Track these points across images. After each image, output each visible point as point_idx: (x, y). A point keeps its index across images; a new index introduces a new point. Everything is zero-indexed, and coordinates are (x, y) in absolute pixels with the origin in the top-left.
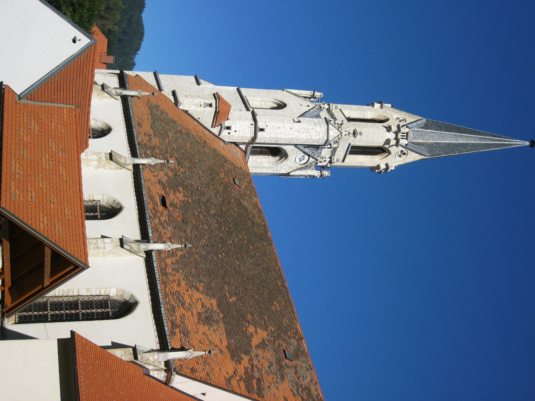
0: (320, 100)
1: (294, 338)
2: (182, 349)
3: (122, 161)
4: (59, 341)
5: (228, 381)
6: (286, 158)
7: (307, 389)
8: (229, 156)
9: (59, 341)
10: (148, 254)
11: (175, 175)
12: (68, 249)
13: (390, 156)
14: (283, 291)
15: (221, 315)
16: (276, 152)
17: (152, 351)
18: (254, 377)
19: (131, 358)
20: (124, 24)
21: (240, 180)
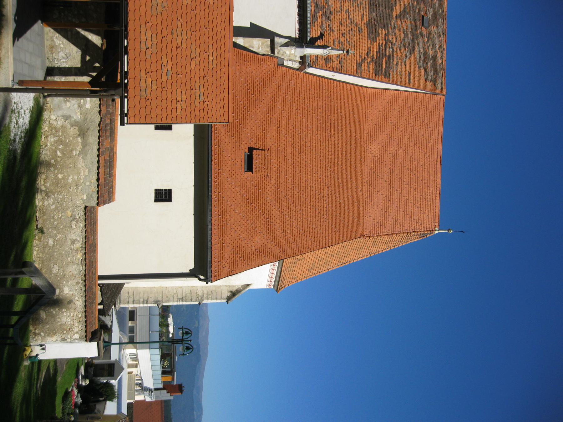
18: (385, 55)
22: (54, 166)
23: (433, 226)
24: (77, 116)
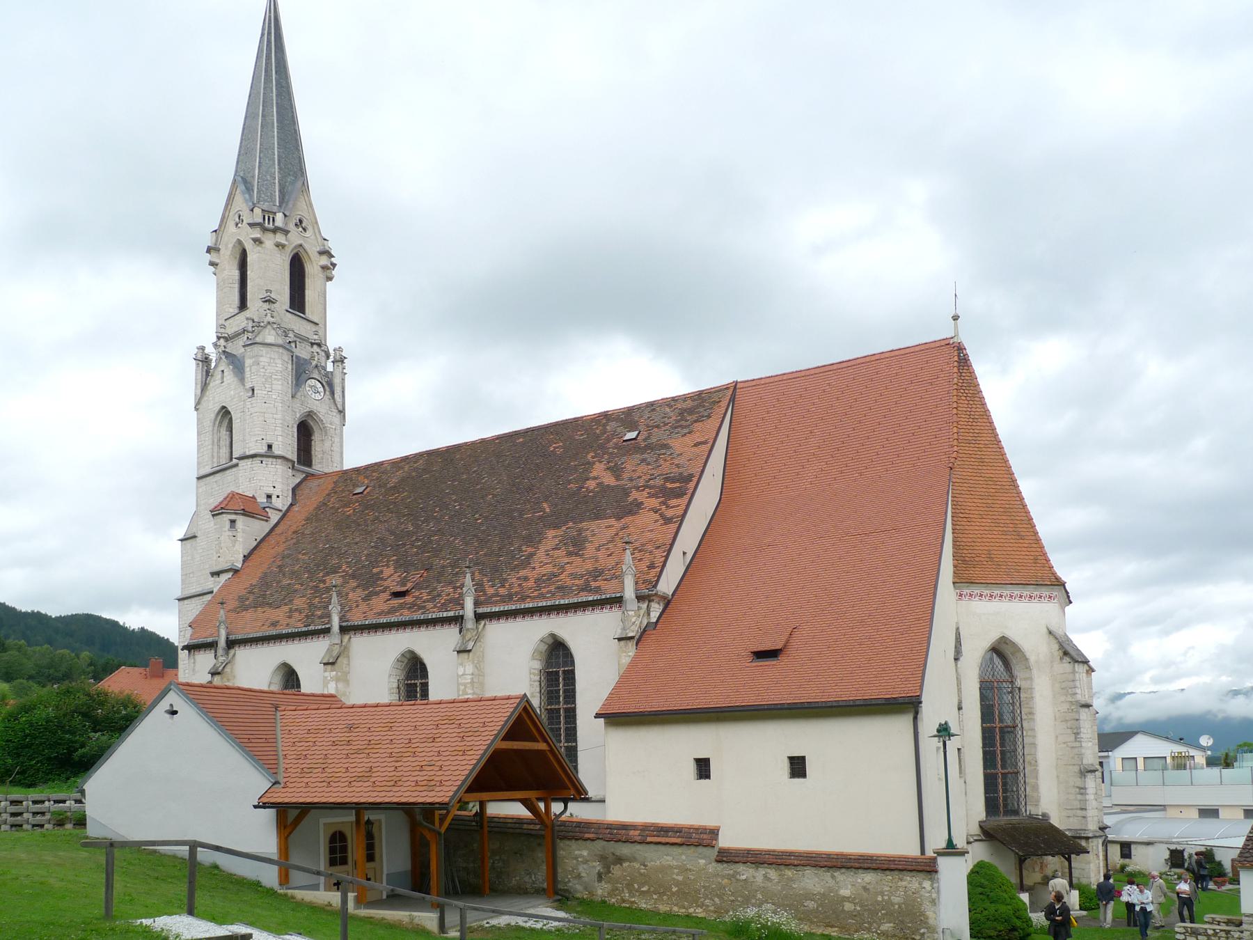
1: (604, 425)
3: (336, 650)
6: (1017, 649)
11: (353, 576)
12: (500, 719)
15: (571, 524)
21: (355, 486)
24: (598, 866)
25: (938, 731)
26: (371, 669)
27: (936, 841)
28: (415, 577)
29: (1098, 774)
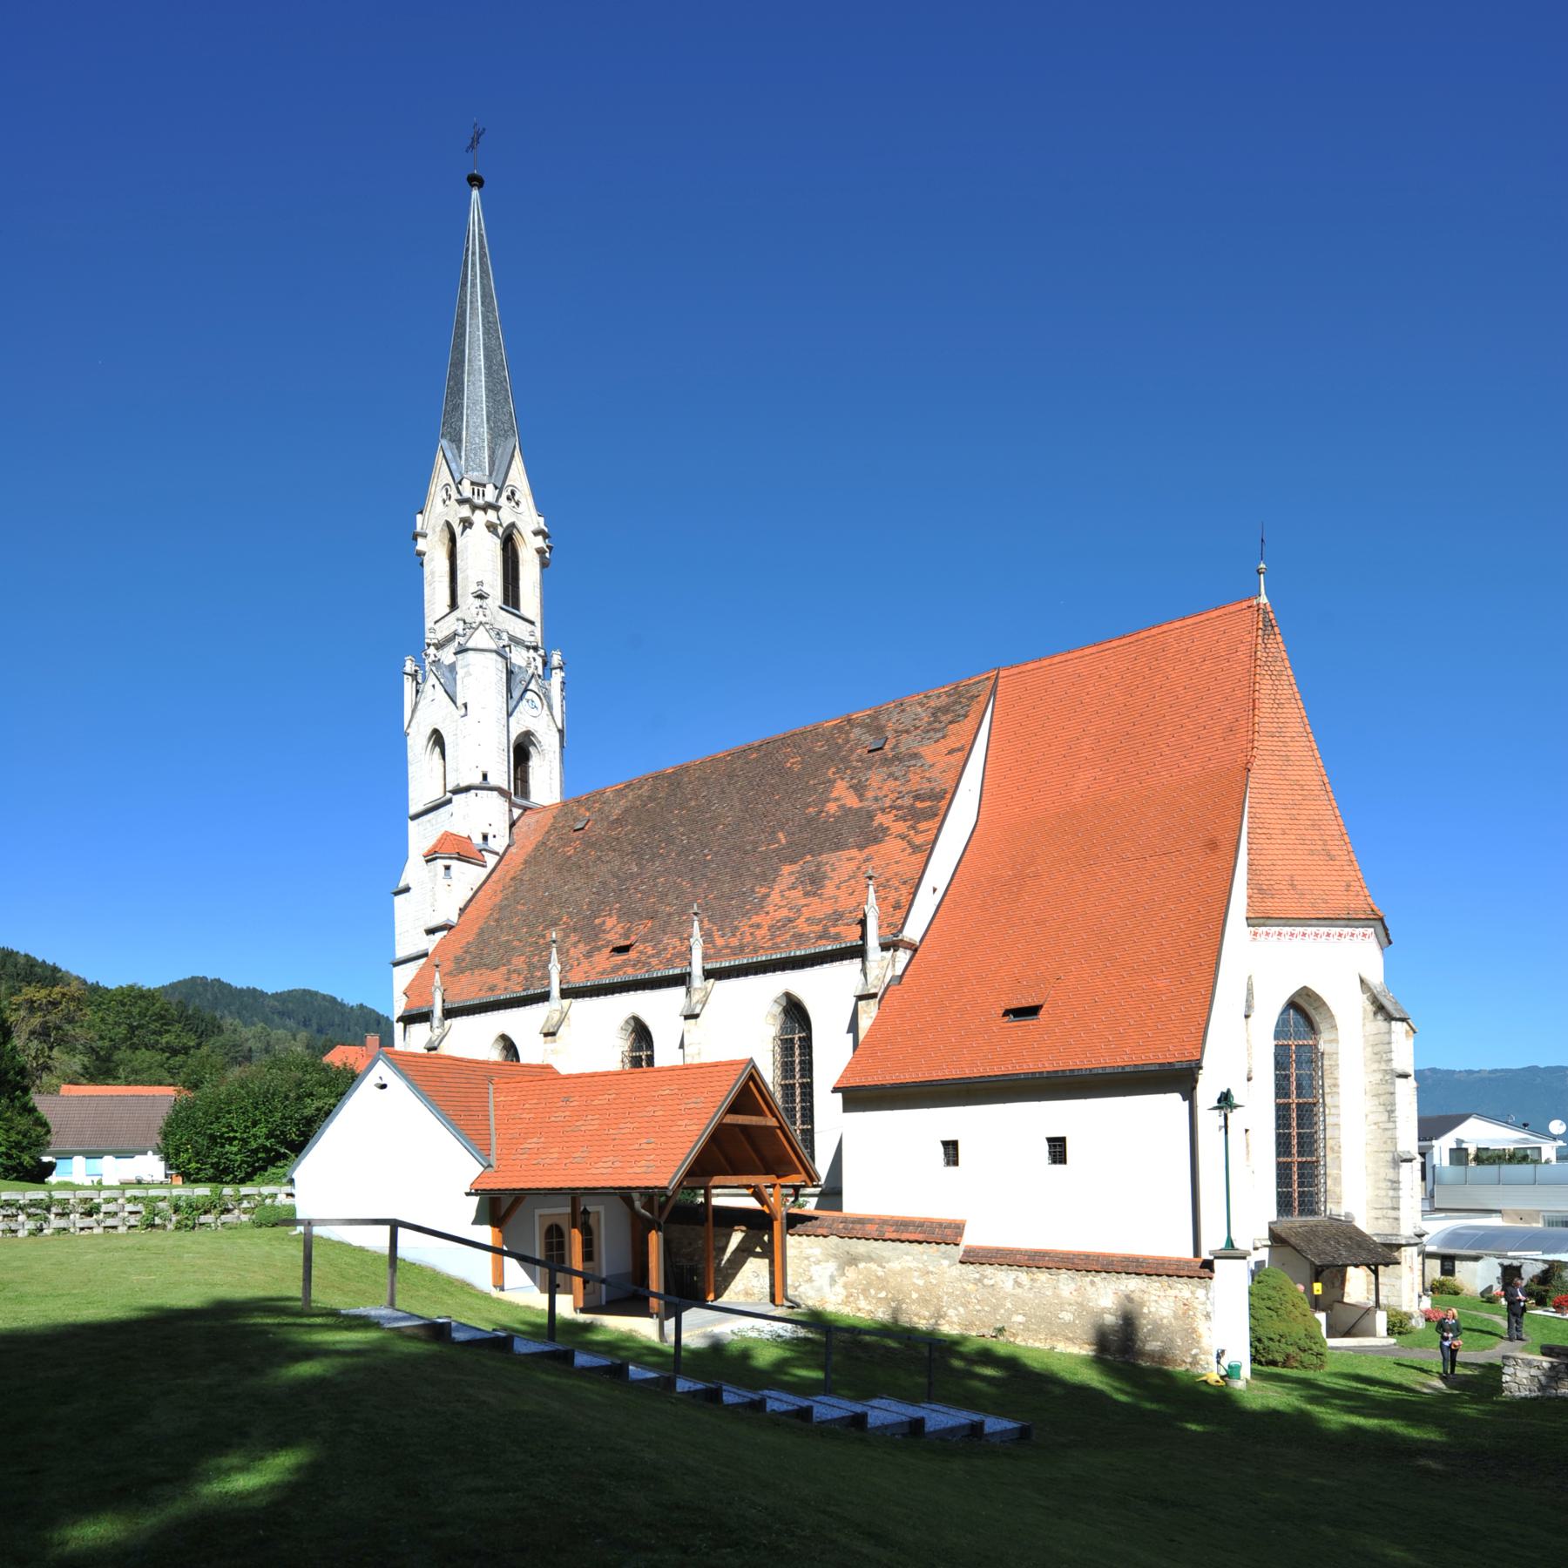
0: (420, 662)
1: (847, 733)
2: (863, 923)
3: (556, 1016)
4: (846, 1110)
5: (916, 849)
6: (1317, 998)
7: (935, 713)
8: (535, 839)
9: (846, 1110)
10: (709, 974)
11: (575, 930)
12: (725, 1090)
13: (519, 524)
14: (768, 749)
15: (809, 858)
16: (522, 752)
17: (864, 971)
18: (912, 805)
19: (873, 1003)
20: (291, 1023)
21: (576, 820)
22: (900, 1302)
23: (1248, 613)
24: (831, 1266)
25: (1219, 1101)
26: (588, 1038)
27: (1212, 1241)
28: (642, 928)
29: (1417, 1164)
